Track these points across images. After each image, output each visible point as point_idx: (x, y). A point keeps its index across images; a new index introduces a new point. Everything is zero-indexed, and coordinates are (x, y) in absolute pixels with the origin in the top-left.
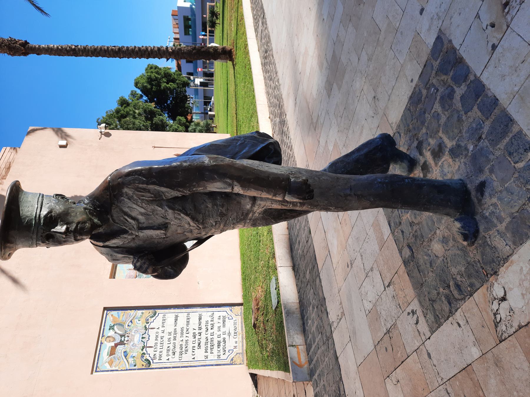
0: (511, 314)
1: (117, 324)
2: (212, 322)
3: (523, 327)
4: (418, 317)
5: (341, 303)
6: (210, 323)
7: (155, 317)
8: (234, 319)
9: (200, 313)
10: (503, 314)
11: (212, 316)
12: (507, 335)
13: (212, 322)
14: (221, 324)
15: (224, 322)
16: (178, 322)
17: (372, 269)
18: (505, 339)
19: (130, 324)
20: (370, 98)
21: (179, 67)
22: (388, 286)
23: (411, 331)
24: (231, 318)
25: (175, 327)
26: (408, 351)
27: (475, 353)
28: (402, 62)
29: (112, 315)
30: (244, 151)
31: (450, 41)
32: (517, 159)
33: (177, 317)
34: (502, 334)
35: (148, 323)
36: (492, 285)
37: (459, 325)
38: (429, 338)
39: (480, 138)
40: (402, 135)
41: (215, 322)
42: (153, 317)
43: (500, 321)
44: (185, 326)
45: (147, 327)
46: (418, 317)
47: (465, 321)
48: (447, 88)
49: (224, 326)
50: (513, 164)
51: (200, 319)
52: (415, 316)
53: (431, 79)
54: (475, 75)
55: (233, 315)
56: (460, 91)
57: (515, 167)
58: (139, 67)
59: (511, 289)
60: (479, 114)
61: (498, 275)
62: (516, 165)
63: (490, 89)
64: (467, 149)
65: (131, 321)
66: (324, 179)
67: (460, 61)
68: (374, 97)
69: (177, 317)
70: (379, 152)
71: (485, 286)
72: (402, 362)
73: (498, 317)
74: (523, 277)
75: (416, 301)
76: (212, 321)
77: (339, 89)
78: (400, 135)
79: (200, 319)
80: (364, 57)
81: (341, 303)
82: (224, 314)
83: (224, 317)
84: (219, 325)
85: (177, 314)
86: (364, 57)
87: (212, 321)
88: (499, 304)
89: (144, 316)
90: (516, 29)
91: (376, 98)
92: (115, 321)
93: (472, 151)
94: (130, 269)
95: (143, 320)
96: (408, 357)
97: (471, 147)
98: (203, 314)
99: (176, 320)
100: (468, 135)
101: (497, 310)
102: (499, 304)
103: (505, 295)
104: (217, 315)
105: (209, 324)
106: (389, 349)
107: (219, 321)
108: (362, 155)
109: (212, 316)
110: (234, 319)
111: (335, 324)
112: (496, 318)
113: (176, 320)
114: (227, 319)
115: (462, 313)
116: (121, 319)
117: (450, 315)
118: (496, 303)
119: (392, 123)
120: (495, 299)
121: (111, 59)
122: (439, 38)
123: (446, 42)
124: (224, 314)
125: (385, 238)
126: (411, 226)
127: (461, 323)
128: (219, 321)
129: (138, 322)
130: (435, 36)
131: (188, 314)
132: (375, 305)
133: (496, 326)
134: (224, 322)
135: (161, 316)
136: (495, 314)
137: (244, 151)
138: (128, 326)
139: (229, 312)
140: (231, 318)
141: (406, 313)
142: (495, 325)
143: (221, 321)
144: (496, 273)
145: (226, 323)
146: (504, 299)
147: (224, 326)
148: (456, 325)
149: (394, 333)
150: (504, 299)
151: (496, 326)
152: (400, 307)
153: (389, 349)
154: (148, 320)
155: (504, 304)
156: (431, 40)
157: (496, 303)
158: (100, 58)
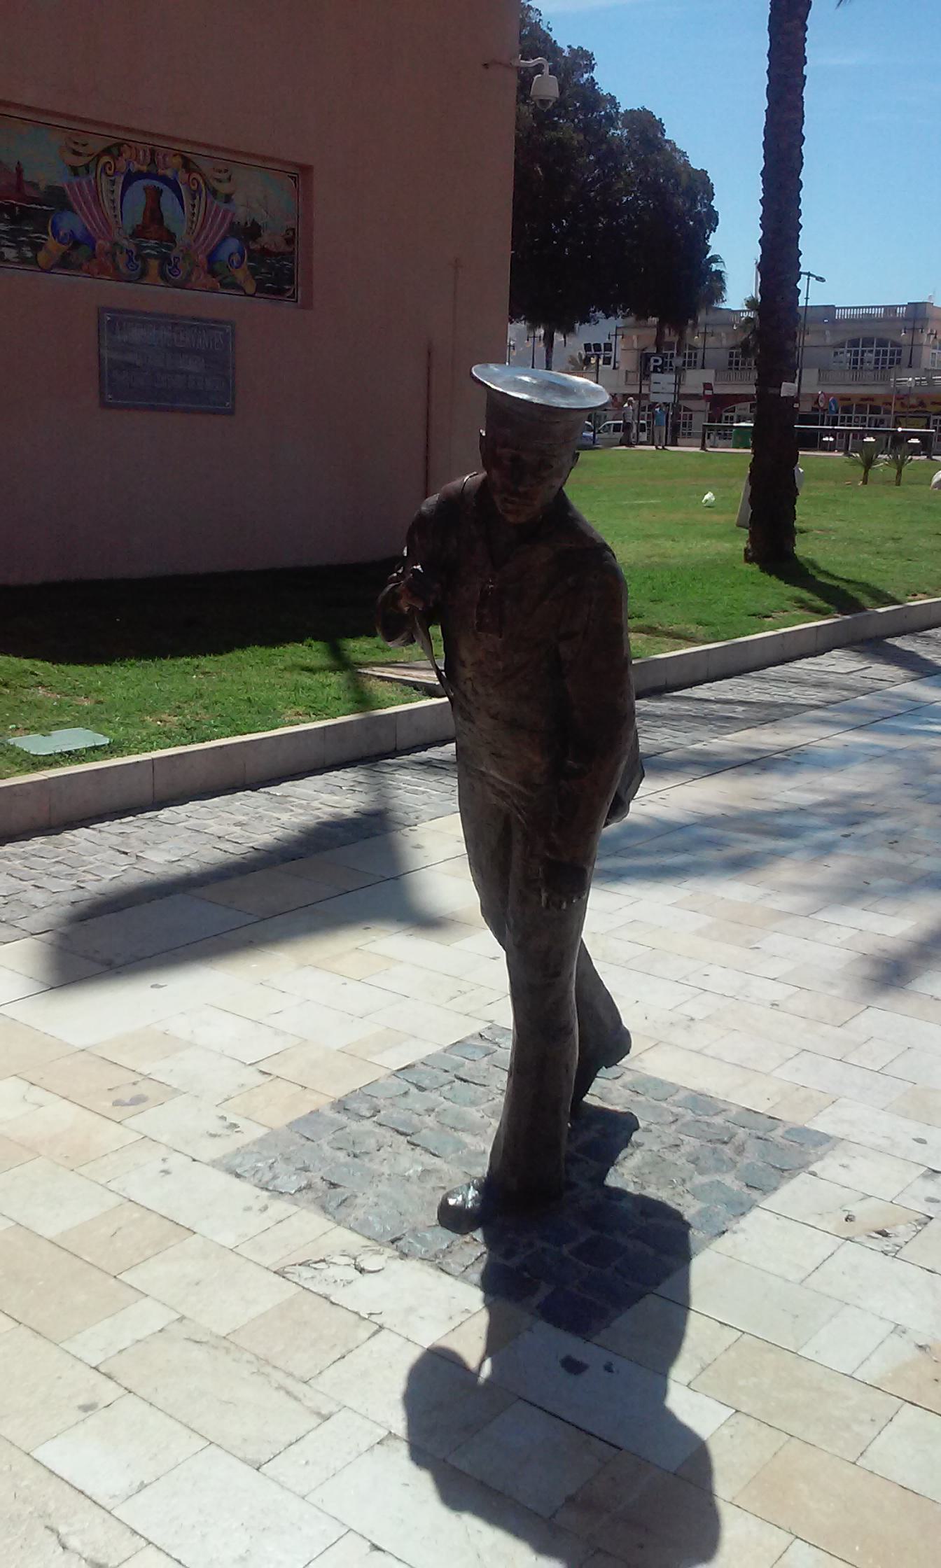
17: (278, 1032)
20: (690, 1009)
30: (624, 763)
31: (821, 1158)
56: (731, 1181)
58: (721, 146)
67: (785, 1173)
68: (692, 1019)
75: (261, 1132)
77: (699, 933)
80: (778, 992)
86: (778, 992)
90: (844, 1249)
91: (691, 1023)
119: (641, 1061)
121: (762, 119)
123: (820, 1150)
125: (375, 1059)
130: (830, 1132)
132: (190, 1044)
137: (624, 763)
144: (404, 1256)
156: (821, 1125)
158: (765, 104)
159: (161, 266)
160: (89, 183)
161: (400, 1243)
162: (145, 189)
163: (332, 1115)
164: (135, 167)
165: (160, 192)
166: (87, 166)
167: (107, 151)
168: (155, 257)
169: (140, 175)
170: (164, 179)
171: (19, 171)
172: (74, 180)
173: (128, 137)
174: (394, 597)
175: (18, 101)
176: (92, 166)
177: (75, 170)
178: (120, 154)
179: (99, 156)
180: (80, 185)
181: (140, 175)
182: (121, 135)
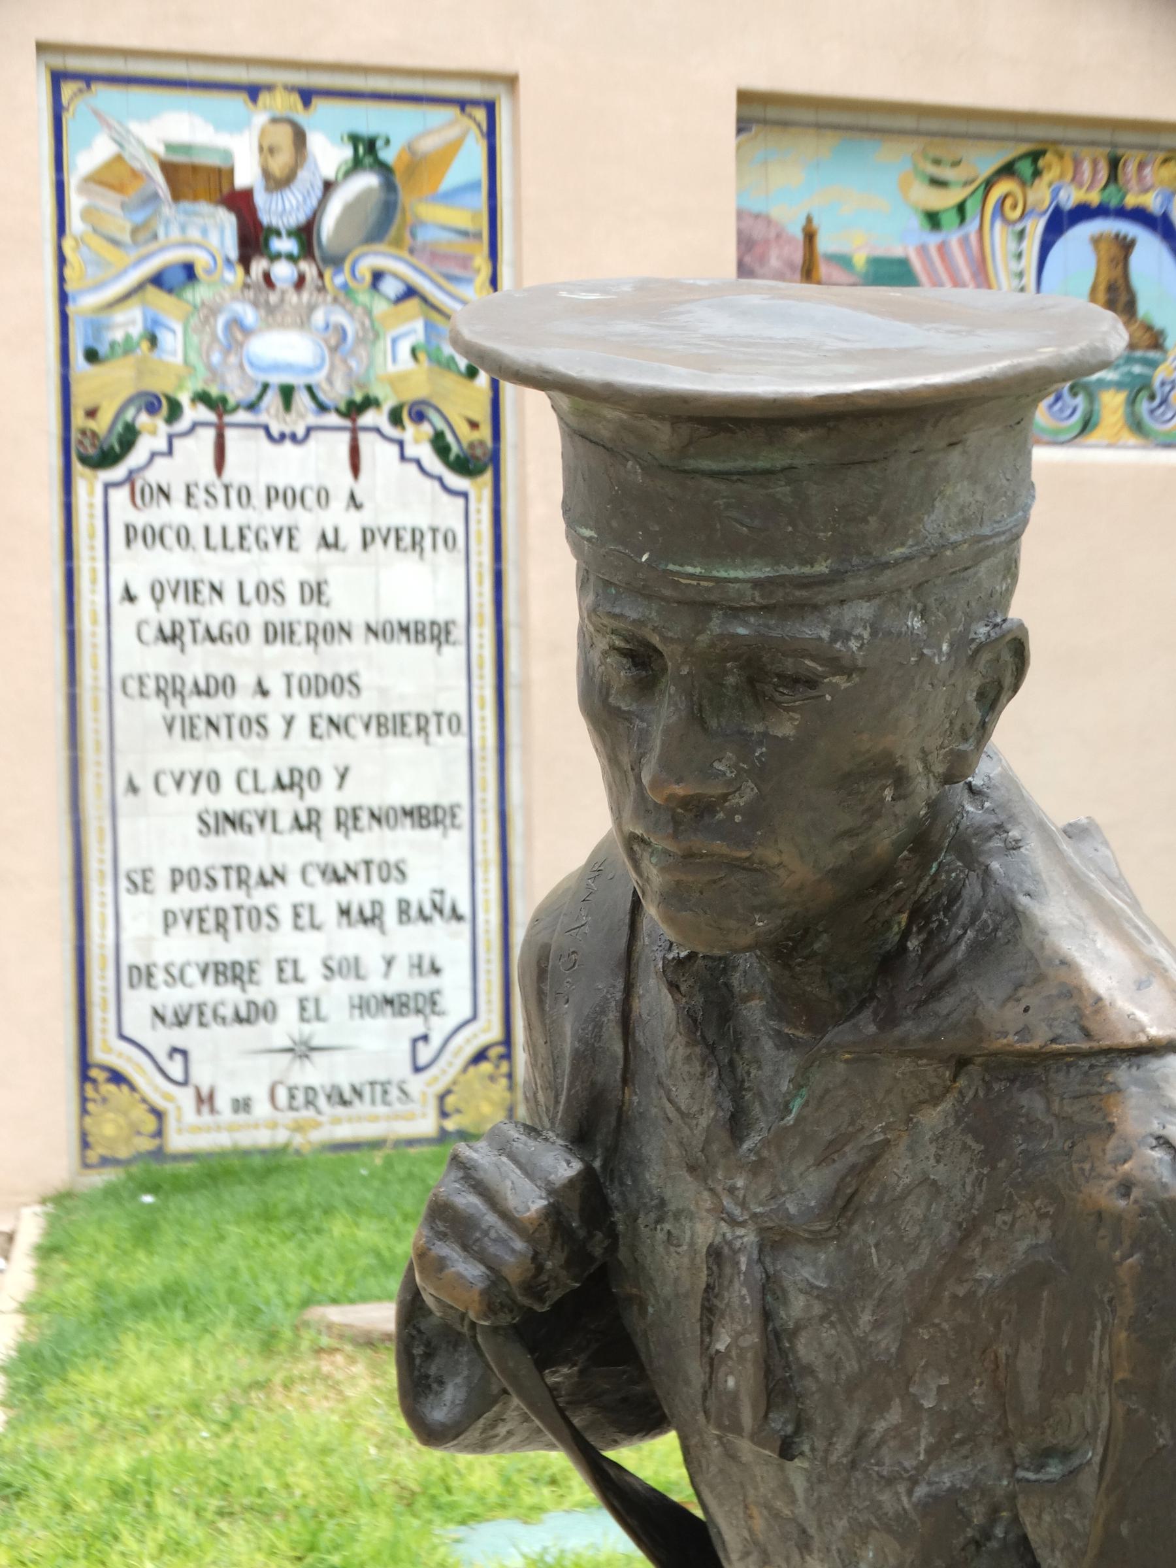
159: (1132, 401)
160: (964, 242)
161: (145, 345)
162: (1096, 241)
163: (816, 1544)
164: (1070, 197)
165: (1126, 246)
166: (961, 208)
167: (1008, 170)
168: (1119, 385)
169: (1083, 213)
170: (1140, 216)
171: (810, 236)
172: (933, 240)
173: (1056, 133)
174: (769, 1151)
175: (627, 921)
176: (971, 208)
177: (933, 219)
178: (1037, 173)
179: (989, 184)
180: (942, 248)
181: (1083, 213)
182: (1040, 132)
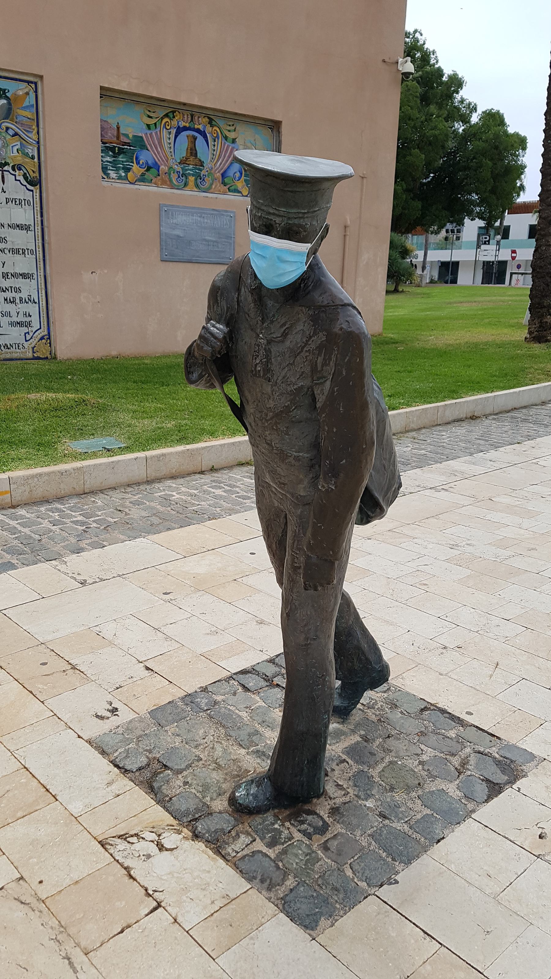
0: (143, 858)
1: (9, 103)
2: (18, 301)
3: (129, 872)
4: (108, 718)
5: (102, 580)
6: (17, 296)
7: (25, 183)
8: (26, 344)
9: (35, 276)
10: (141, 847)
11: (30, 300)
12: (111, 851)
13: (18, 301)
14: (15, 319)
15: (20, 324)
16: (17, 231)
17: (168, 638)
18: (106, 849)
19: (11, 132)
20: (443, 640)
21: (526, 208)
22: (148, 668)
23: (82, 704)
24: (28, 337)
25: (6, 226)
26: (50, 701)
27: (76, 808)
28: (500, 697)
29: (27, 94)
32: (356, 867)
33: (27, 228)
34: (112, 845)
35: (14, 169)
36: (179, 832)
37: (109, 784)
38: (79, 737)
39: (385, 817)
40: (386, 695)
41: (20, 306)
42: (26, 178)
43: (129, 842)
44: (9, 246)
45: (6, 168)
46: (108, 718)
47: (118, 792)
48: (456, 769)
49: (12, 324)
50: (349, 862)
51: (24, 276)
52: (108, 714)
53: (472, 744)
54: (473, 811)
55: (34, 342)
57: (345, 864)
59: (176, 858)
60: (419, 816)
61: (193, 840)
62: (348, 865)
63: (453, 831)
64: (368, 797)
65: (16, 134)
66: (331, 601)
68: (445, 648)
69: (27, 228)
70: (362, 666)
71: (175, 822)
72: (31, 692)
73: (134, 840)
74: (196, 874)
75: (132, 716)
76: (21, 299)
78: (385, 692)
79: (24, 276)
81: (102, 580)
82: (36, 325)
83: (28, 324)
84: (13, 314)
85: (32, 228)
87: (21, 299)
88: (152, 841)
89: (27, 160)
91: (444, 651)
92: (15, 99)
93: (365, 806)
94: (118, 128)
95: (20, 159)
96: (42, 702)
97: (370, 804)
98: (34, 282)
99: (20, 227)
100: (388, 800)
101: (143, 838)
102: (152, 841)
103: (167, 850)
104: (33, 309)
105: (14, 294)
106: (46, 670)
107: (21, 314)
108: (358, 641)
109: (30, 300)
110: (26, 344)
111: (62, 567)
112: (132, 836)
113: (20, 227)
114: (25, 330)
115: (128, 788)
116: (20, 112)
117: (123, 770)
118: (154, 837)
120: (159, 836)
122: (532, 757)
124: (36, 325)
126: (247, 708)
127: (113, 787)
128: (21, 314)
129: (15, 149)
131: (32, 252)
133: (120, 837)
134: (20, 324)
135: (28, 196)
136: (136, 835)
138: (7, 128)
139: (39, 334)
140: (28, 337)
141: (110, 698)
142: (122, 835)
143: (21, 318)
145: (17, 328)
146: (161, 847)
147: (12, 324)
148: (110, 779)
149: (73, 677)
150: (161, 847)
151: (120, 837)
152: (117, 688)
153: (46, 670)
154: (20, 169)
155: (153, 849)
157: (154, 837)
